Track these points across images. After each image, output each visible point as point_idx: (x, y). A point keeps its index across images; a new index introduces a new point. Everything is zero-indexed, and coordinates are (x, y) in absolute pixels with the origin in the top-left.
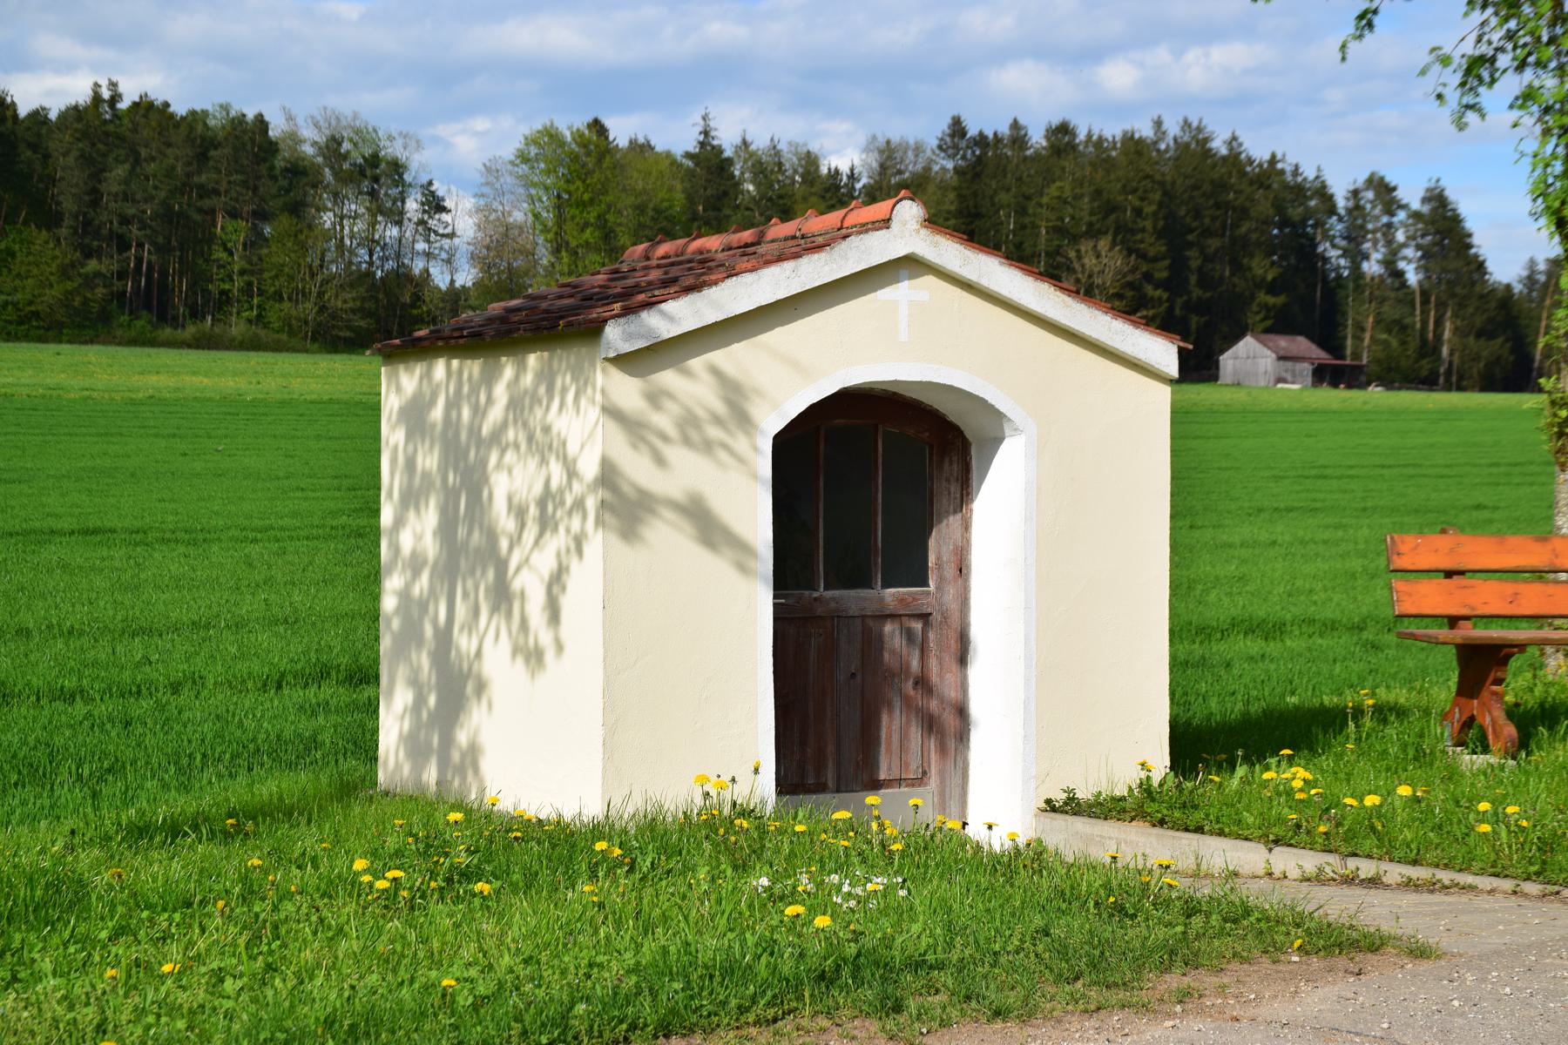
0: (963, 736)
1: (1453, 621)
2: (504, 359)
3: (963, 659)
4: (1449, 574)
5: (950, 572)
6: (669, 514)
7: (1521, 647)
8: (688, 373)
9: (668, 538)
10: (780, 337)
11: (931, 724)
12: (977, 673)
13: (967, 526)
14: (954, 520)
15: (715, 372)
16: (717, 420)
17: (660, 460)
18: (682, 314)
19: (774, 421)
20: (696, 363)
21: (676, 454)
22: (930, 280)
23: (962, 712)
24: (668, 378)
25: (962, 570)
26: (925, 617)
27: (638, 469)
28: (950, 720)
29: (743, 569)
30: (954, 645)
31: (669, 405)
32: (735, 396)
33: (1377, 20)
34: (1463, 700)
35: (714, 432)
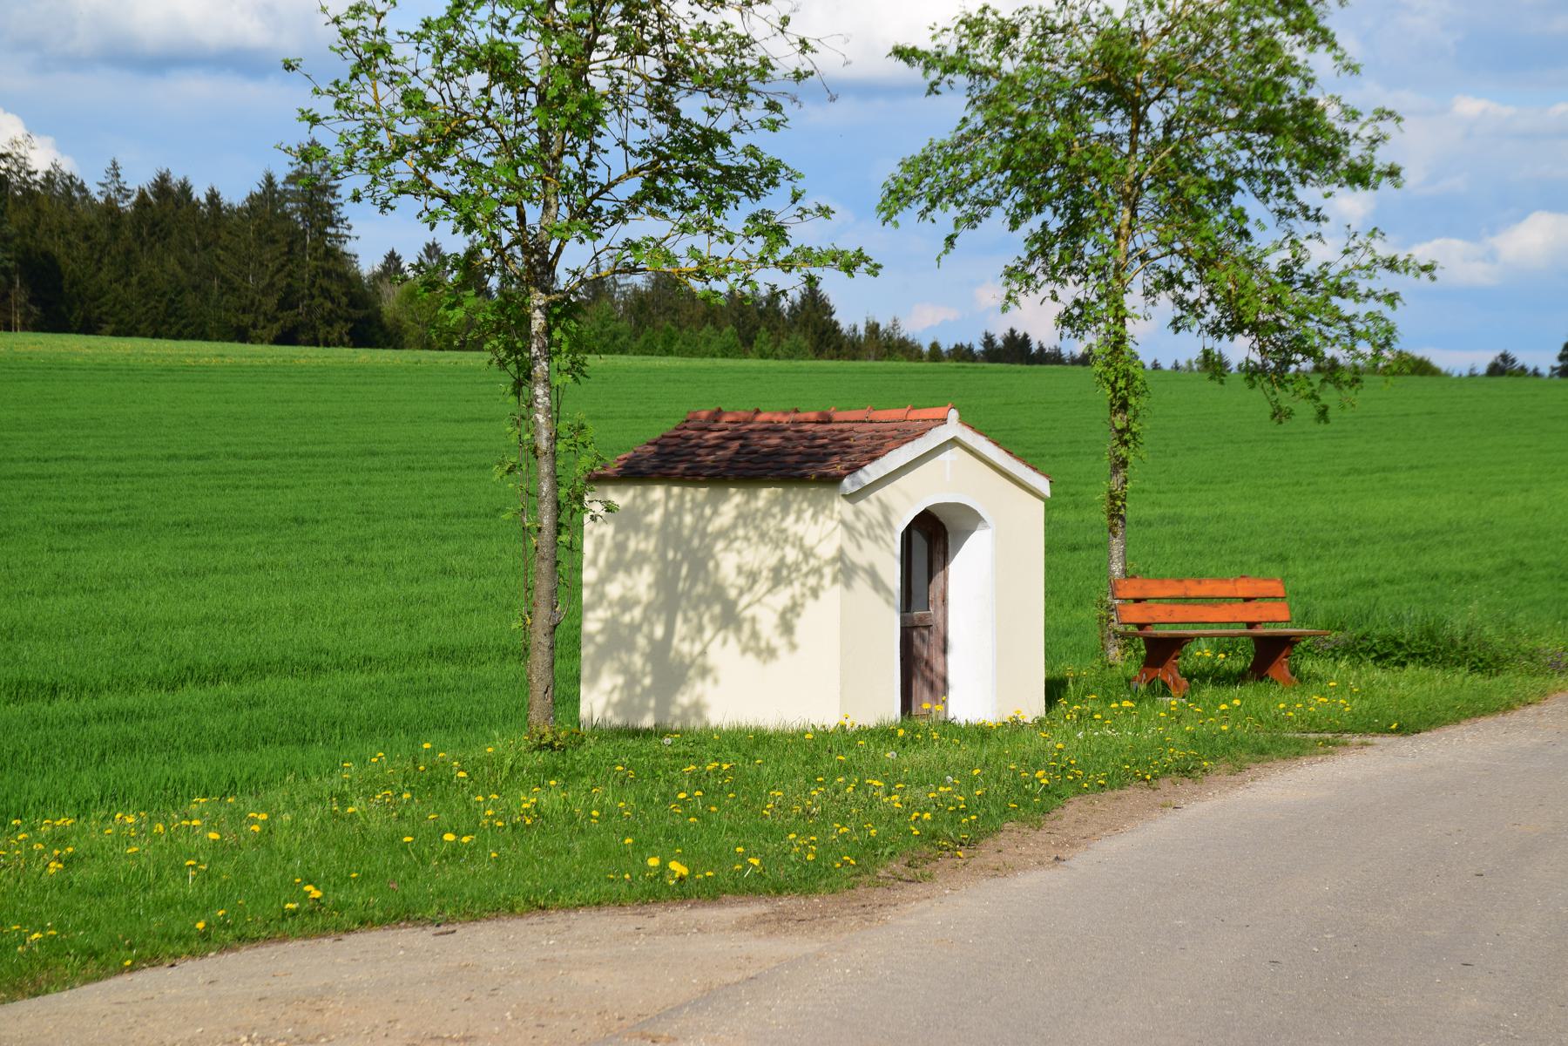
0: (945, 692)
1: (1251, 625)
2: (733, 490)
3: (945, 651)
4: (1137, 601)
5: (939, 602)
6: (861, 574)
7: (1190, 638)
8: (869, 501)
9: (861, 584)
10: (902, 482)
11: (932, 687)
12: (952, 658)
13: (946, 578)
14: (941, 574)
15: (879, 500)
16: (880, 525)
17: (859, 547)
18: (872, 472)
19: (901, 527)
20: (872, 496)
21: (865, 543)
22: (957, 449)
23: (945, 680)
24: (862, 504)
25: (944, 600)
26: (928, 627)
27: (852, 553)
28: (939, 684)
29: (888, 602)
30: (941, 643)
31: (863, 518)
32: (886, 510)
33: (956, 241)
34: (1149, 670)
35: (879, 532)
